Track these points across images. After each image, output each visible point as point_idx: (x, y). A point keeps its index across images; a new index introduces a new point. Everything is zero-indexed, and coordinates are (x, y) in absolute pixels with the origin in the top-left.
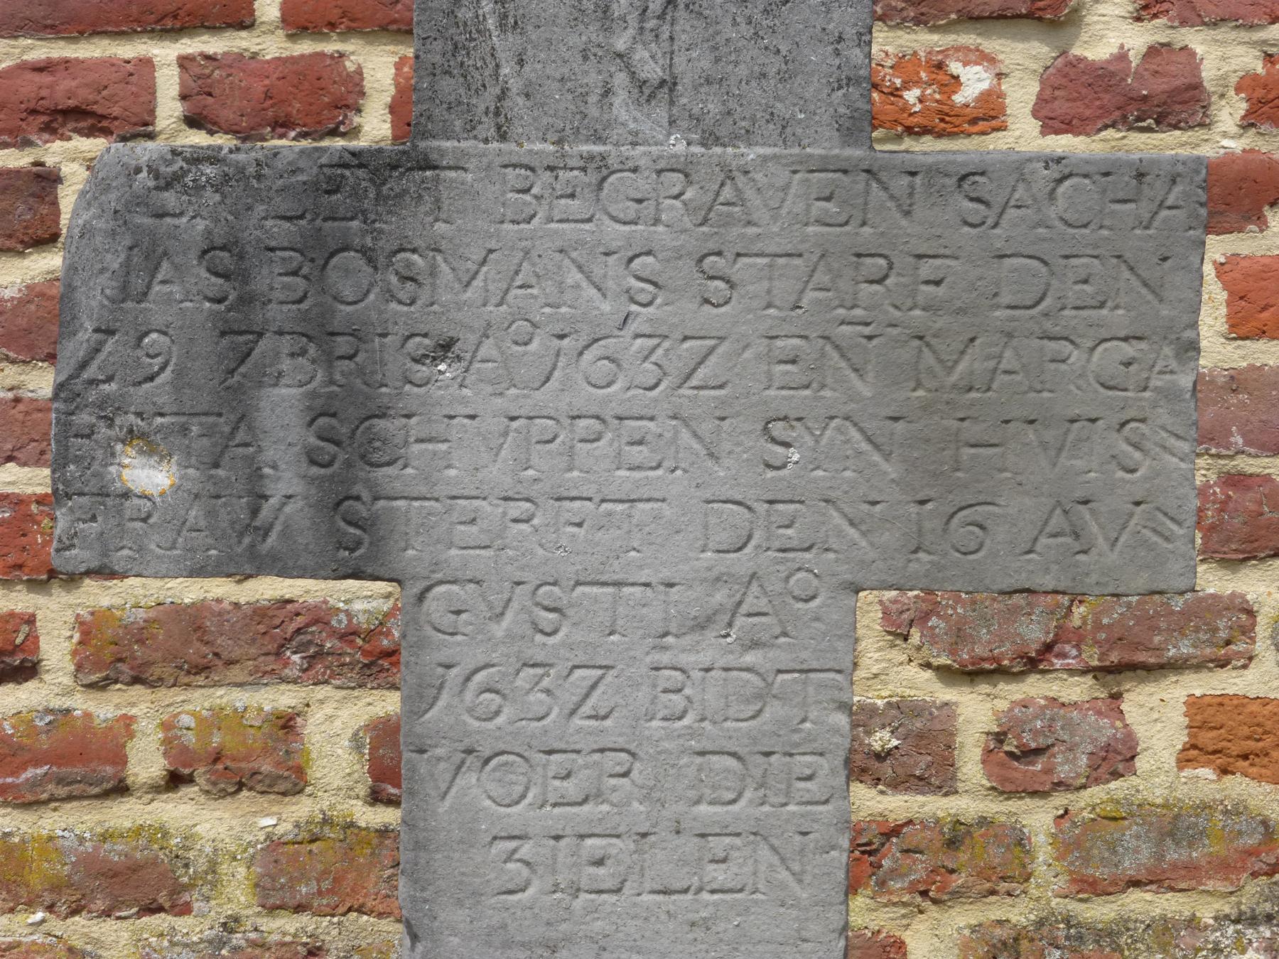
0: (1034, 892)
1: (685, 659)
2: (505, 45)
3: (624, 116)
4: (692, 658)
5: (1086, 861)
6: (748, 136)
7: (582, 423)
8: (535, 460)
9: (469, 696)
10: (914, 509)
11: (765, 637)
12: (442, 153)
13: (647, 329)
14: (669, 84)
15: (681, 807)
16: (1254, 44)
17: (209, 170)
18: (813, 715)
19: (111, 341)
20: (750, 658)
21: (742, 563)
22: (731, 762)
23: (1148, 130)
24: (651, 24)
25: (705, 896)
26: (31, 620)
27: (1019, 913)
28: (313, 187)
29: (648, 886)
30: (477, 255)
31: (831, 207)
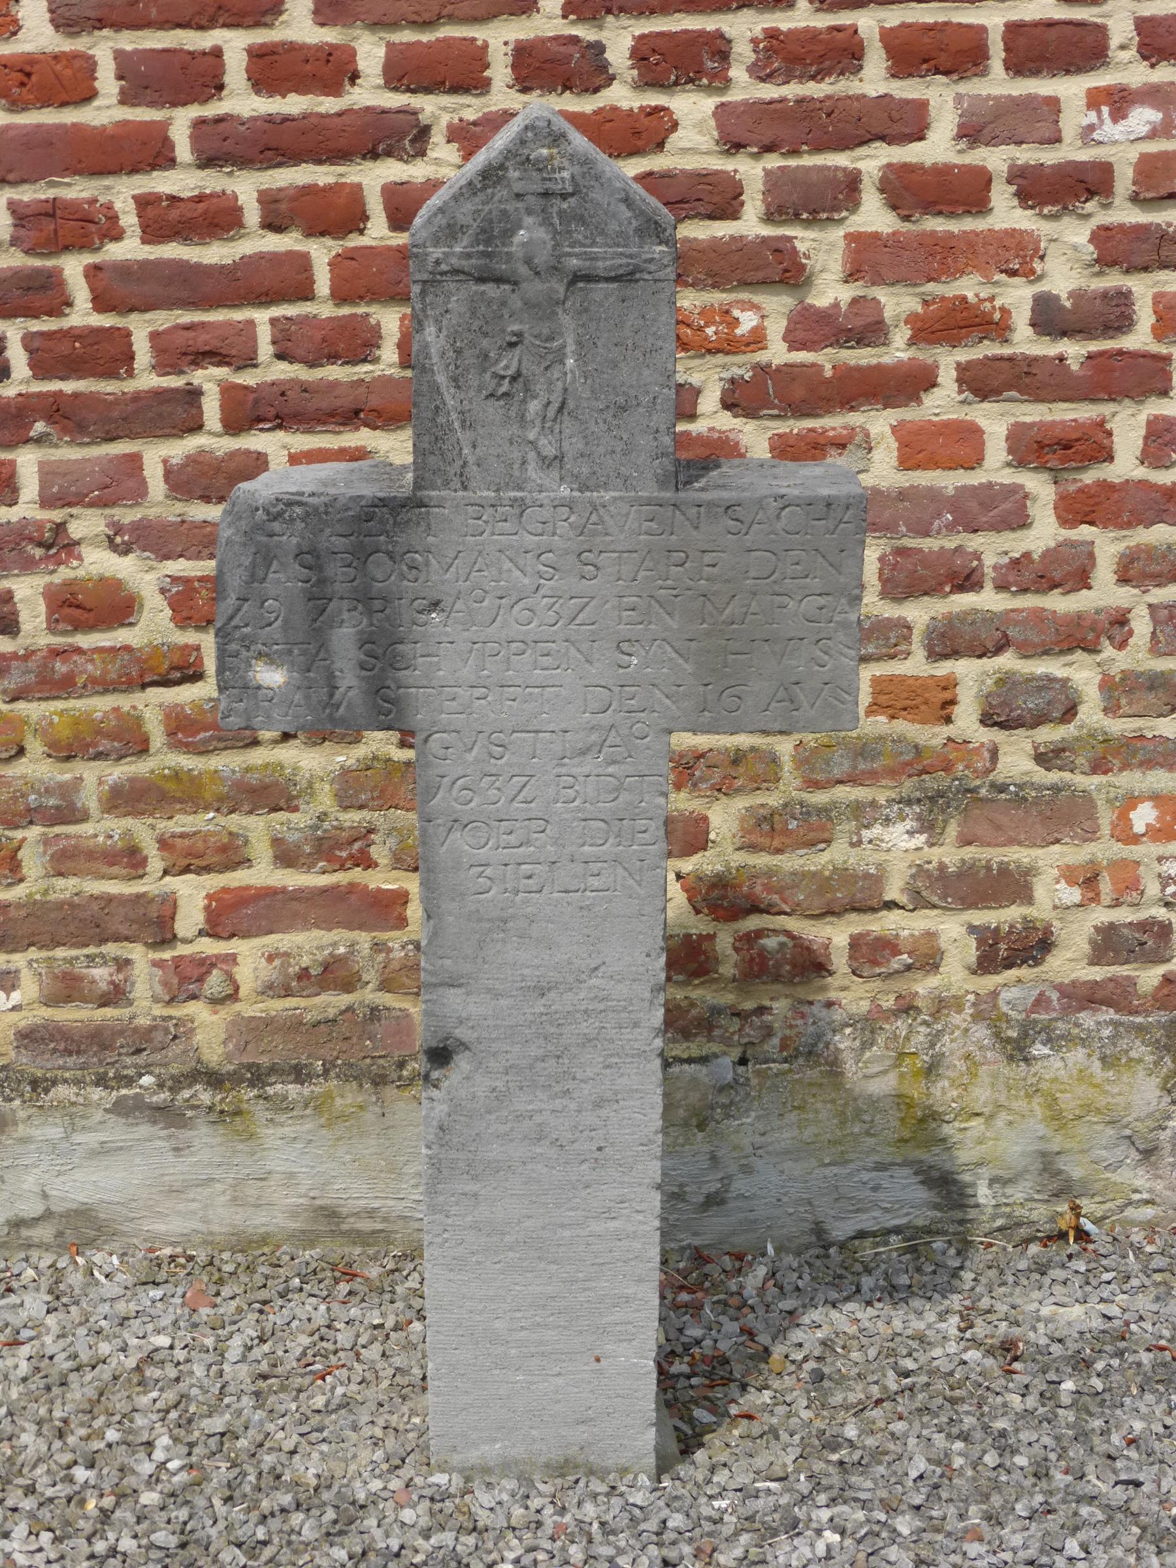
0: (782, 788)
1: (574, 771)
2: (464, 437)
3: (534, 476)
4: (579, 770)
5: (812, 770)
6: (606, 486)
7: (514, 645)
8: (488, 666)
9: (454, 792)
10: (701, 688)
11: (619, 758)
12: (431, 498)
13: (549, 593)
14: (560, 458)
15: (574, 848)
16: (917, 295)
17: (298, 510)
18: (647, 798)
19: (246, 605)
20: (610, 770)
21: (606, 719)
22: (602, 824)
23: (852, 347)
24: (548, 425)
25: (588, 893)
26: (198, 648)
27: (773, 800)
28: (357, 519)
29: (556, 888)
30: (452, 555)
31: (653, 525)
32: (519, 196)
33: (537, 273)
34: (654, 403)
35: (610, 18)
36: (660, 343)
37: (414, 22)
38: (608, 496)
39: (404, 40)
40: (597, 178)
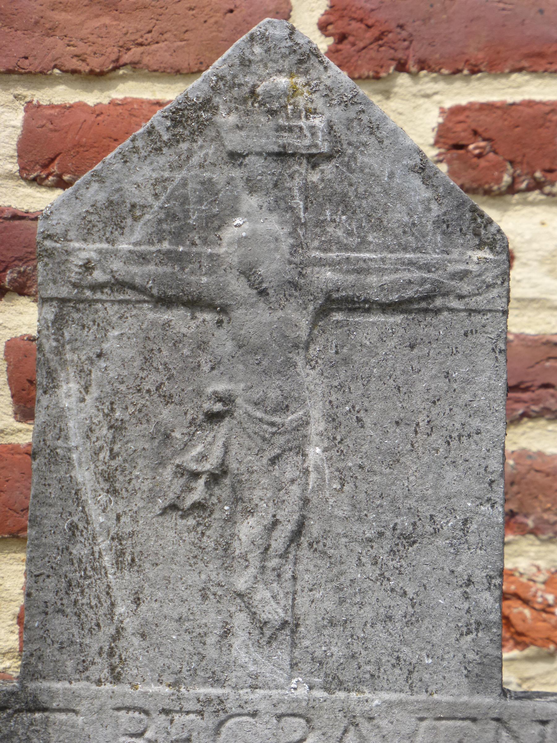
2: (121, 583)
3: (243, 658)
6: (373, 681)
12: (52, 694)
14: (291, 626)
24: (273, 563)
32: (235, 157)
33: (263, 293)
34: (465, 531)
35: (403, 79)
36: (476, 423)
37: (74, 72)
38: (377, 699)
39: (57, 100)
40: (373, 129)
